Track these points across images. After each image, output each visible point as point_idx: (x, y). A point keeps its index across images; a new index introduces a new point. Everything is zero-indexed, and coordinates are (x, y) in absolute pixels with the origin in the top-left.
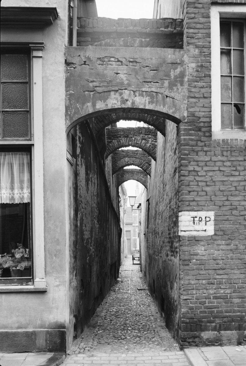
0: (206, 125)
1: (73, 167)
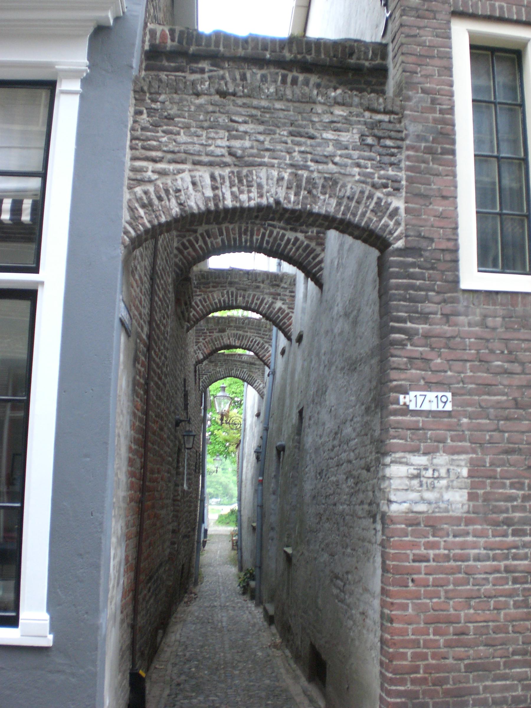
0: (448, 257)
1: (131, 339)
